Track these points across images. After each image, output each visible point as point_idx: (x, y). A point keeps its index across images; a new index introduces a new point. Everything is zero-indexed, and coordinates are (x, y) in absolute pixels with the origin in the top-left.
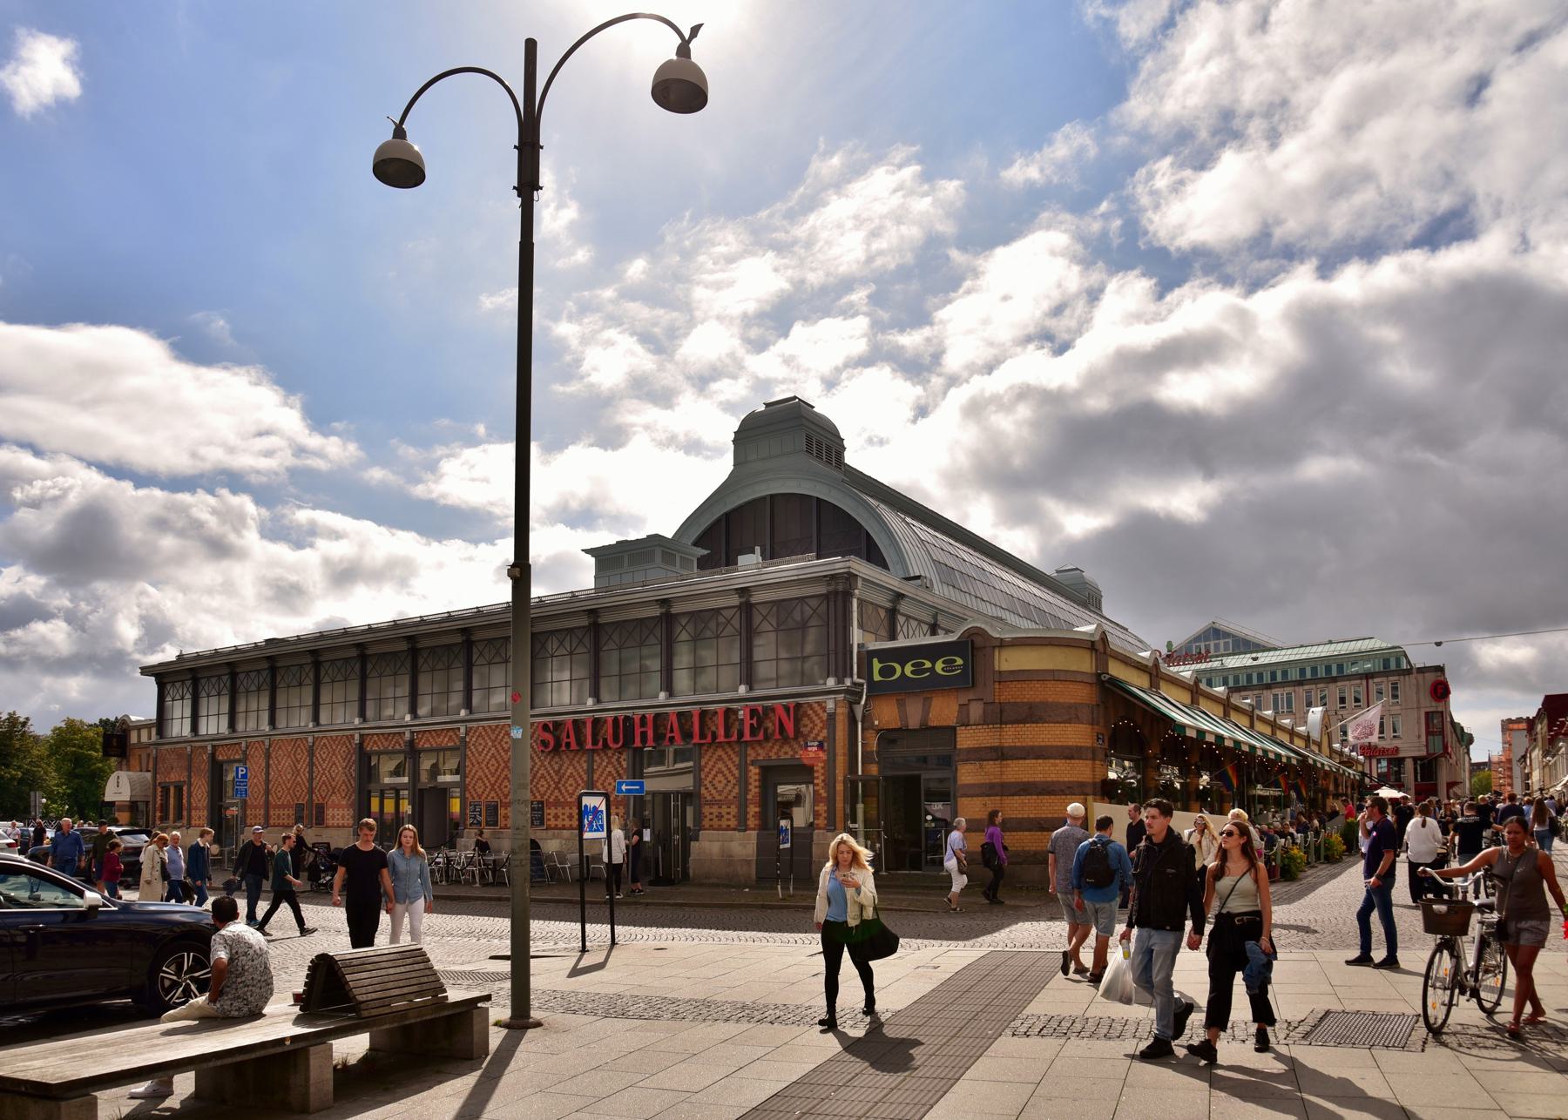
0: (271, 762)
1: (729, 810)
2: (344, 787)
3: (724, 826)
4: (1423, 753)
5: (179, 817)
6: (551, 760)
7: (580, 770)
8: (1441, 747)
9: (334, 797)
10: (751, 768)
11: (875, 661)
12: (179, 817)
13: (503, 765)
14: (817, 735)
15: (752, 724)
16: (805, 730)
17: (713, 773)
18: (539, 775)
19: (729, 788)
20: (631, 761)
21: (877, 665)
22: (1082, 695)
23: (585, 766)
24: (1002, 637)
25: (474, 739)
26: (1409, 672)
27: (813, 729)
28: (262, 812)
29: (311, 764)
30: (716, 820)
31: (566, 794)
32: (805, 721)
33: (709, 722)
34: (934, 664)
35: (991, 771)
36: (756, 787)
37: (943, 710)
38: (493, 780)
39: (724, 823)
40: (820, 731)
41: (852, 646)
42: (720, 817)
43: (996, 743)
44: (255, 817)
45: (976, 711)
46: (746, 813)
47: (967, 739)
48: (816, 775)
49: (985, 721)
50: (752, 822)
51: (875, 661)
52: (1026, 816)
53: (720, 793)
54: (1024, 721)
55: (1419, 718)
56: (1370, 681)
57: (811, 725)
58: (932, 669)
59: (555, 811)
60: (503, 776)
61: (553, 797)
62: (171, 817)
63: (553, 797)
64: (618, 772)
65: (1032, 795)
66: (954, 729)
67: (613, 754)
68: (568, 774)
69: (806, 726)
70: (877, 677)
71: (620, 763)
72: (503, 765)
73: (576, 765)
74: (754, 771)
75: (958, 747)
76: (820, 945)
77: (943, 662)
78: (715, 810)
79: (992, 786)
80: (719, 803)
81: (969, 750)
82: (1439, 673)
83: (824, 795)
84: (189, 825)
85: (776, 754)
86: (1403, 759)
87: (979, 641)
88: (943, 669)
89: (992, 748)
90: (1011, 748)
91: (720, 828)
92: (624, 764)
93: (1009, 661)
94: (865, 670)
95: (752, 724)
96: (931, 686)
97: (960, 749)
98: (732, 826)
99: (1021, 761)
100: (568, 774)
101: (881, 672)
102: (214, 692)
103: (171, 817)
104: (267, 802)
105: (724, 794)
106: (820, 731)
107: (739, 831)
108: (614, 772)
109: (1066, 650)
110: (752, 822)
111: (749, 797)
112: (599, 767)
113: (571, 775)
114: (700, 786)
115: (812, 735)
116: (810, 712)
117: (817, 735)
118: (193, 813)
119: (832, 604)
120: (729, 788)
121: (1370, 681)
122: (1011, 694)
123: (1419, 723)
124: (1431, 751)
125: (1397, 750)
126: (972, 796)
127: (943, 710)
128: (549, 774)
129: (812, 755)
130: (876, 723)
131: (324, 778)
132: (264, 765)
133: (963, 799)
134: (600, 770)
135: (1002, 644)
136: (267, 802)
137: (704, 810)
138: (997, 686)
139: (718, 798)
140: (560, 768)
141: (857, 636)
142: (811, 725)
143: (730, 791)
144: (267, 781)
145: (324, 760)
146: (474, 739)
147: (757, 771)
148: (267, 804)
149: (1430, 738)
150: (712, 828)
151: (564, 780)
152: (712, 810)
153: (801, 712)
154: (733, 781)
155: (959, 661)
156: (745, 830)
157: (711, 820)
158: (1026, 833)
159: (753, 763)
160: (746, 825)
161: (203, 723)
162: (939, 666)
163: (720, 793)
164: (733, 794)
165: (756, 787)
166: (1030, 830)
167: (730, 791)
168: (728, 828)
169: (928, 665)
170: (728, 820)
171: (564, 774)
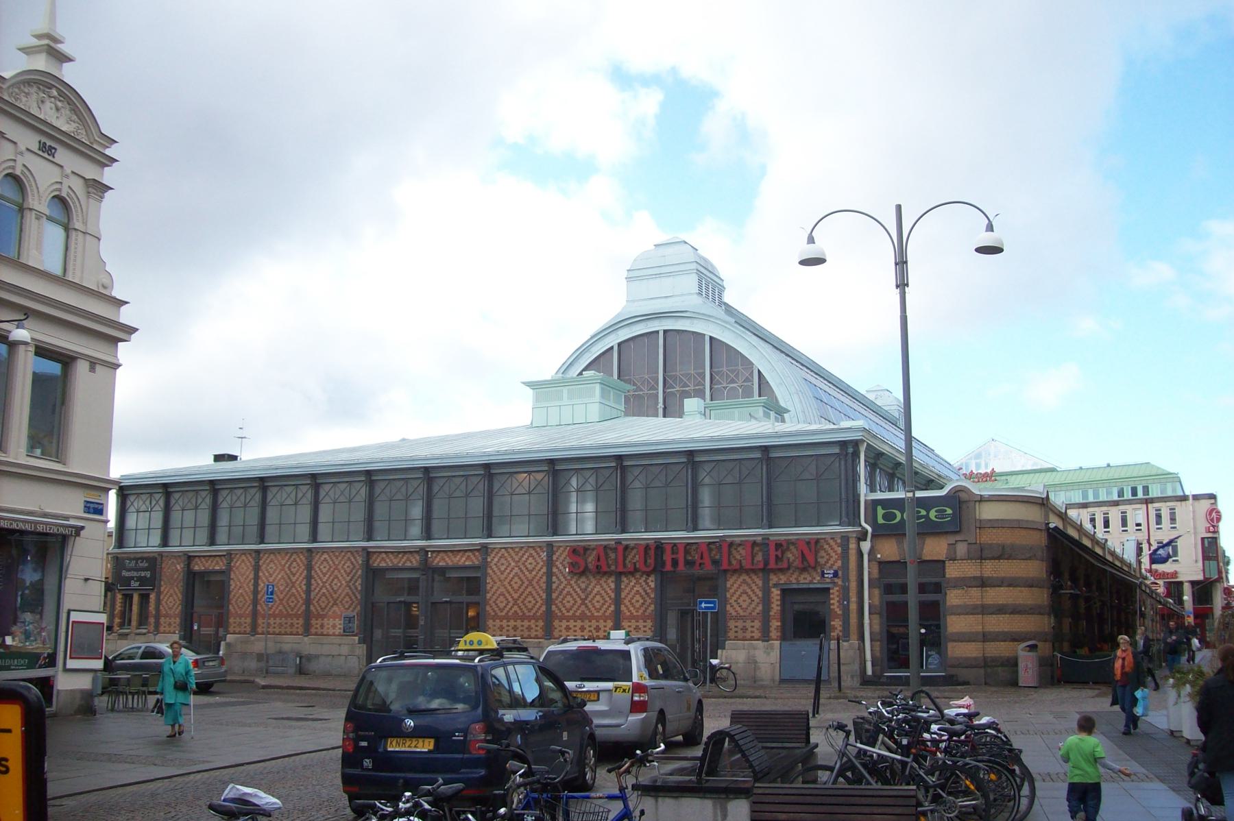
0: (261, 574)
1: (753, 624)
2: (347, 599)
3: (749, 637)
4: (1200, 577)
5: (143, 621)
6: (577, 580)
7: (608, 589)
8: (1216, 572)
9: (335, 608)
10: (773, 590)
11: (879, 508)
12: (143, 621)
13: (527, 583)
14: (833, 565)
15: (777, 556)
16: (822, 561)
17: (738, 593)
18: (565, 592)
19: (753, 606)
20: (659, 582)
21: (880, 512)
22: (1041, 540)
23: (613, 586)
24: (982, 494)
25: (496, 560)
26: (1184, 498)
27: (828, 560)
28: (249, 620)
29: (309, 578)
30: (740, 631)
31: (563, 609)
32: (822, 553)
33: (734, 552)
34: (928, 513)
35: (974, 596)
36: (777, 605)
37: (935, 548)
38: (516, 596)
39: (294, 630)
40: (835, 562)
41: (859, 495)
42: (744, 629)
43: (978, 574)
44: (240, 624)
45: (962, 549)
46: (769, 627)
47: (952, 571)
48: (831, 596)
49: (969, 557)
50: (774, 633)
51: (879, 508)
52: (1001, 630)
53: (745, 610)
54: (999, 558)
55: (1196, 544)
56: (1150, 505)
57: (828, 557)
58: (927, 517)
59: (528, 624)
60: (527, 592)
61: (579, 612)
62: (134, 623)
63: (579, 612)
64: (645, 591)
65: (1005, 614)
66: (944, 562)
67: (642, 576)
68: (595, 592)
69: (822, 557)
70: (880, 521)
71: (647, 583)
72: (527, 583)
73: (332, 565)
74: (776, 593)
75: (947, 576)
76: (49, 813)
77: (936, 511)
78: (740, 624)
79: (975, 607)
80: (743, 618)
81: (957, 579)
82: (1213, 501)
83: (840, 612)
84: (157, 630)
85: (796, 579)
86: (1181, 583)
87: (963, 496)
88: (936, 517)
89: (975, 578)
90: (989, 577)
91: (744, 639)
92: (653, 585)
93: (988, 512)
94: (872, 519)
95: (777, 556)
96: (930, 530)
97: (949, 578)
98: (756, 638)
99: (997, 588)
100: (595, 592)
101: (884, 517)
102: (189, 506)
103: (134, 623)
104: (308, 610)
105: (749, 611)
106: (835, 562)
107: (763, 641)
108: (641, 591)
109: (1026, 505)
110: (774, 633)
111: (772, 613)
112: (626, 586)
113: (598, 593)
114: (726, 605)
115: (829, 565)
116: (826, 546)
117: (833, 565)
118: (162, 620)
119: (843, 463)
120: (753, 606)
121: (1150, 505)
122: (988, 537)
123: (1195, 547)
124: (1207, 576)
125: (1175, 574)
126: (959, 614)
127: (935, 548)
128: (509, 592)
129: (828, 580)
130: (879, 556)
131: (324, 590)
132: (252, 576)
133: (952, 616)
134: (628, 589)
135: (982, 499)
136: (308, 610)
137: (729, 624)
138: (978, 531)
139: (742, 614)
140: (587, 587)
141: (863, 488)
142: (828, 557)
143: (754, 609)
144: (308, 592)
145: (324, 575)
146: (496, 560)
147: (779, 592)
148: (255, 614)
149: (1206, 562)
150: (736, 638)
151: (591, 597)
152: (737, 624)
153: (818, 547)
154: (757, 600)
155: (949, 511)
156: (768, 641)
157: (736, 632)
158: (1002, 643)
159: (775, 585)
160: (768, 636)
161: (174, 535)
162: (933, 514)
163: (745, 610)
164: (757, 611)
165: (777, 605)
166: (1005, 641)
167: (754, 609)
168: (752, 639)
169: (923, 513)
170: (752, 632)
171: (591, 592)
